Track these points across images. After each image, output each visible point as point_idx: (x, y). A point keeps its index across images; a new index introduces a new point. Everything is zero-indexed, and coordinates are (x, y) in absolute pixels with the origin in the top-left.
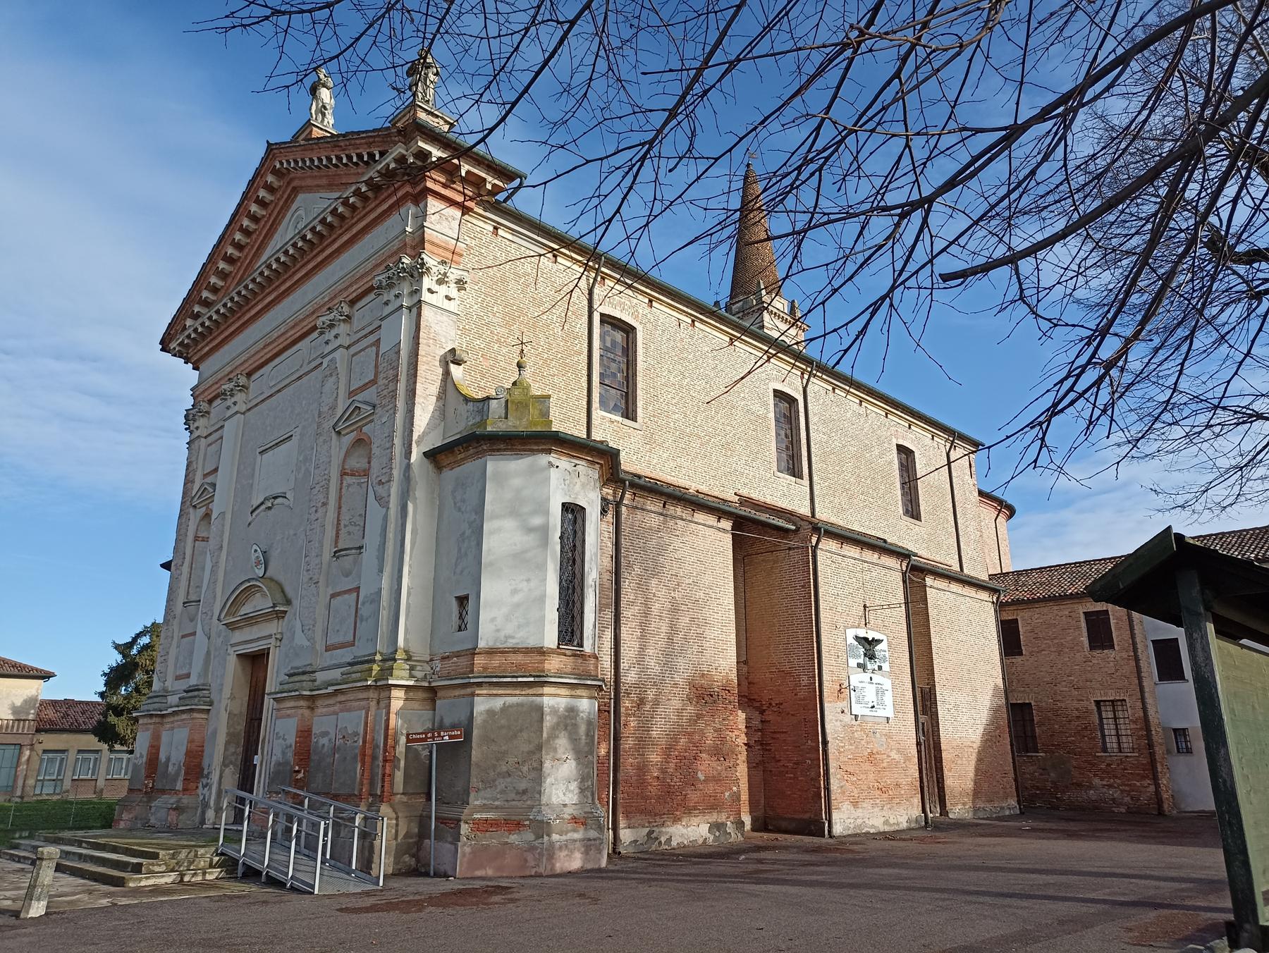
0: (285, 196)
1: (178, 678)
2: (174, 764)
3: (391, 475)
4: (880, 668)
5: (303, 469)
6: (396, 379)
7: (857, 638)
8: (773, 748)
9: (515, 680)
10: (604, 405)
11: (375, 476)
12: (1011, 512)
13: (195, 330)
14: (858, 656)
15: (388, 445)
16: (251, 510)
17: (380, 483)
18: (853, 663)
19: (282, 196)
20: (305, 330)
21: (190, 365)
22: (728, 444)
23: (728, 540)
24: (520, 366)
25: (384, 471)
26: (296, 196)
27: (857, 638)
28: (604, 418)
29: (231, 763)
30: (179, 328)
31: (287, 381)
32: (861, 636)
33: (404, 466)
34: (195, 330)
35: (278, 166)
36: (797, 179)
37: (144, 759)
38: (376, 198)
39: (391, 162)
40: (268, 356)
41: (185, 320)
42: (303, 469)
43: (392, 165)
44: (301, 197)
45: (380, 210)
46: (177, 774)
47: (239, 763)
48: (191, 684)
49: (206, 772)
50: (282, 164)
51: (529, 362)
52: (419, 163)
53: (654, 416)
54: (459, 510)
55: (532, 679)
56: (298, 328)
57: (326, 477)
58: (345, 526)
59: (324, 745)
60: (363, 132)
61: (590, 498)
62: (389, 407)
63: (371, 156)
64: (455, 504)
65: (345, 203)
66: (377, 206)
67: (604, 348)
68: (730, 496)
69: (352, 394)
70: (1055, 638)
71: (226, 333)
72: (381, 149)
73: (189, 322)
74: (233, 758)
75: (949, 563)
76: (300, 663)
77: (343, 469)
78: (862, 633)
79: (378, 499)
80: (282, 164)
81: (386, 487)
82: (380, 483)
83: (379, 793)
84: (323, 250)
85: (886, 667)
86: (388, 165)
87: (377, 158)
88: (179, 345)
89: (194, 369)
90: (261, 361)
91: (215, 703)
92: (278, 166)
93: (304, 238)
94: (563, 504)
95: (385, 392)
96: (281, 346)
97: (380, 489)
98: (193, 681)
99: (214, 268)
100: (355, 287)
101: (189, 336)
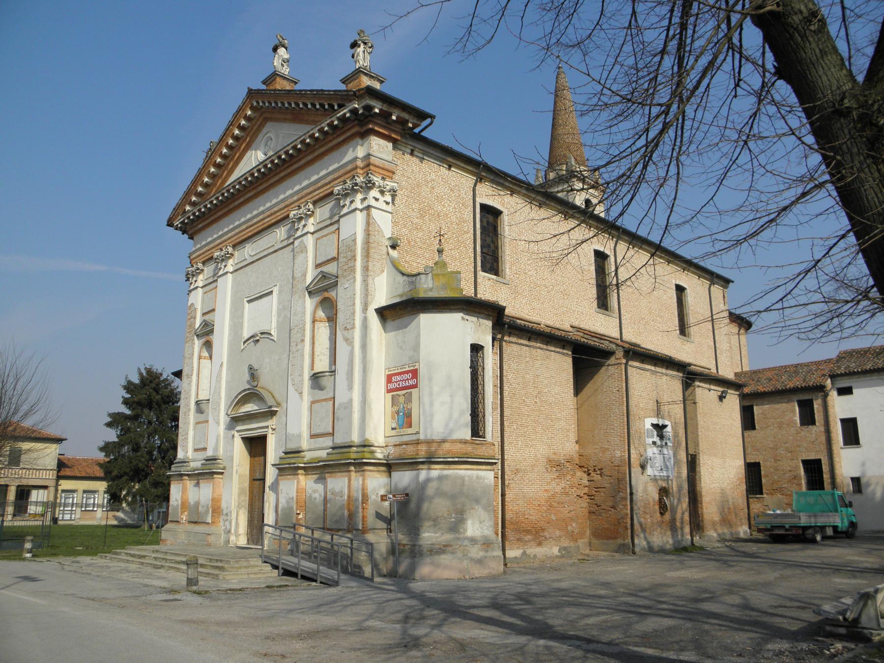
0: (259, 123)
1: (196, 450)
2: (203, 506)
3: (354, 324)
4: (666, 444)
5: (282, 315)
6: (354, 258)
7: (653, 425)
8: (596, 498)
9: (445, 460)
10: (484, 270)
11: (341, 324)
12: (726, 282)
13: (194, 214)
14: (653, 437)
15: (350, 304)
16: (243, 340)
17: (346, 329)
18: (650, 441)
19: (256, 124)
20: (279, 218)
21: (186, 236)
22: (565, 290)
23: (570, 360)
24: (440, 251)
25: (348, 321)
26: (266, 123)
27: (653, 425)
28: (484, 277)
29: (243, 506)
30: (181, 211)
31: (265, 253)
32: (655, 423)
33: (362, 318)
34: (194, 214)
35: (255, 104)
36: (646, 151)
37: (180, 502)
38: (333, 133)
40: (250, 234)
41: (185, 206)
42: (282, 315)
43: (348, 115)
44: (268, 124)
45: (335, 142)
46: (207, 512)
47: (247, 506)
48: (208, 455)
49: (225, 512)
50: (258, 103)
51: (446, 247)
52: (367, 113)
53: (516, 274)
54: (401, 348)
55: (457, 459)
56: (273, 216)
58: (318, 356)
59: (316, 498)
60: (326, 91)
61: (486, 339)
63: (331, 106)
64: (398, 344)
65: (312, 136)
66: (334, 139)
67: (482, 227)
68: (567, 327)
69: (318, 266)
70: (778, 418)
71: (216, 216)
72: (340, 102)
73: (188, 208)
74: (243, 503)
75: (709, 367)
76: (292, 446)
77: (314, 317)
78: (655, 421)
79: (346, 340)
80: (258, 103)
81: (350, 332)
82: (346, 329)
83: (360, 528)
84: (291, 165)
85: (669, 444)
86: (345, 114)
87: (336, 107)
88: (180, 223)
89: (189, 238)
90: (244, 237)
91: (227, 468)
92: (255, 104)
93: (279, 157)
94: (471, 345)
95: (346, 267)
96: (260, 228)
97: (346, 333)
98: (210, 453)
99: (207, 171)
100: (317, 192)
101: (188, 218)
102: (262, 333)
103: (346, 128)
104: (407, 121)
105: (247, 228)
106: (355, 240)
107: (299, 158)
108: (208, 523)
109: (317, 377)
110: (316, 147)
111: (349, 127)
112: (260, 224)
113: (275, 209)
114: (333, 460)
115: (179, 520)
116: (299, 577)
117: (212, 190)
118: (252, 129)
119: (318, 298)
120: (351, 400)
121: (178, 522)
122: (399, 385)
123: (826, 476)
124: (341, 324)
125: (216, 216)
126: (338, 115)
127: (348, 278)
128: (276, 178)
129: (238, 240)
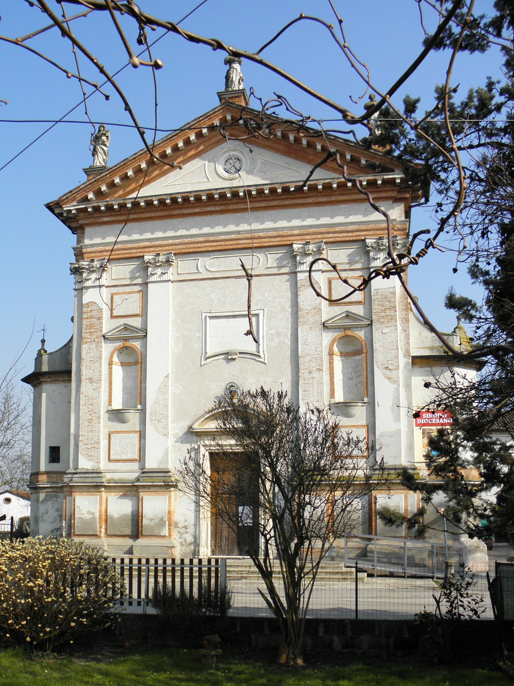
2: (151, 520)
11: (380, 363)
30: (79, 197)
39: (398, 178)
57: (318, 352)
62: (390, 325)
99: (136, 165)
102: (240, 353)
103: (383, 189)
104: (376, 181)
105: (205, 242)
106: (394, 293)
107: (307, 195)
108: (165, 536)
109: (347, 406)
110: (336, 193)
111: (387, 189)
112: (234, 242)
113: (261, 234)
114: (80, 482)
115: (98, 534)
116: (376, 576)
117: (130, 185)
118: (209, 139)
119: (336, 334)
120: (399, 432)
121: (96, 535)
122: (432, 421)
123: (374, 530)
124: (380, 363)
125: (141, 216)
126: (385, 177)
127: (386, 325)
128: (263, 204)
129: (184, 251)
